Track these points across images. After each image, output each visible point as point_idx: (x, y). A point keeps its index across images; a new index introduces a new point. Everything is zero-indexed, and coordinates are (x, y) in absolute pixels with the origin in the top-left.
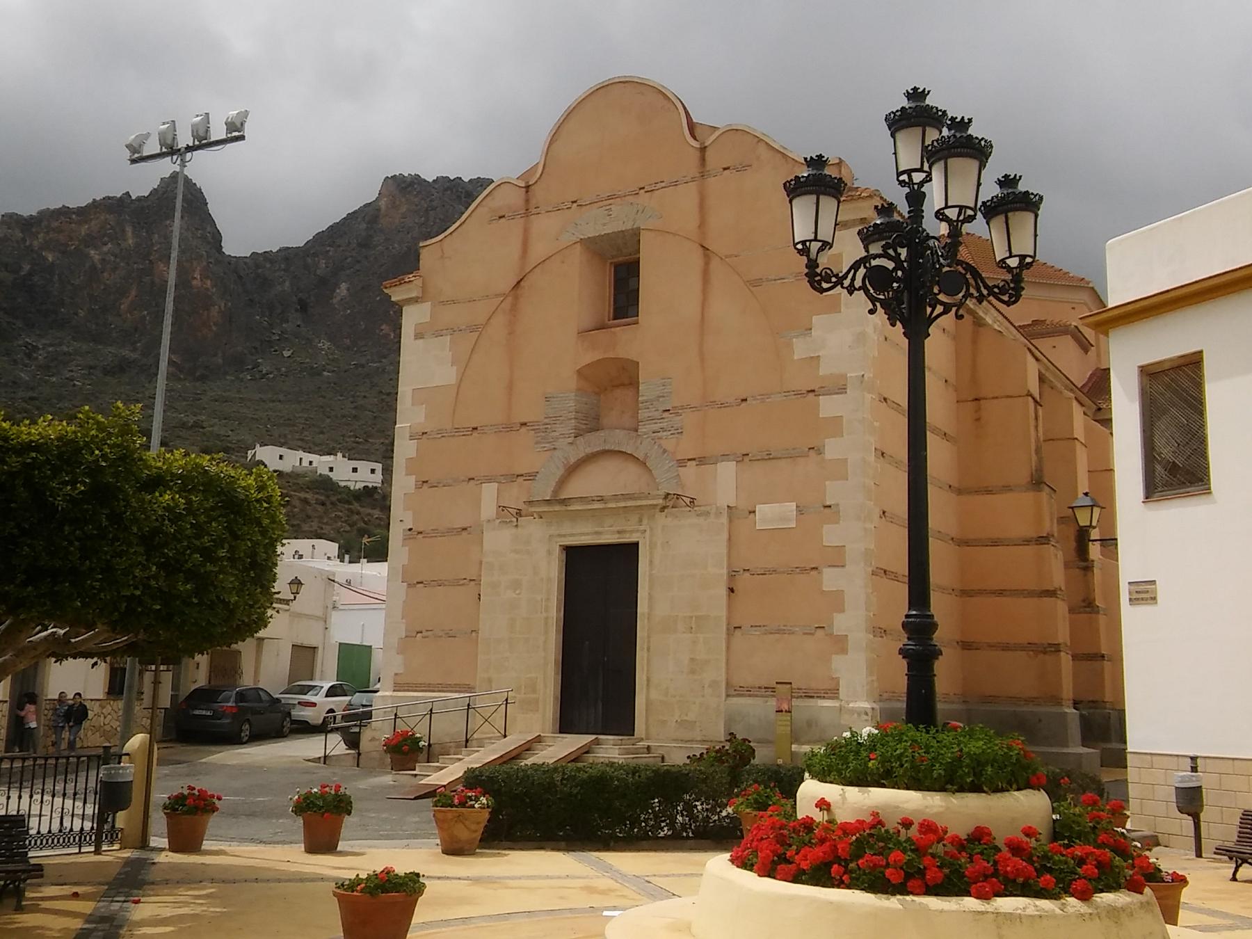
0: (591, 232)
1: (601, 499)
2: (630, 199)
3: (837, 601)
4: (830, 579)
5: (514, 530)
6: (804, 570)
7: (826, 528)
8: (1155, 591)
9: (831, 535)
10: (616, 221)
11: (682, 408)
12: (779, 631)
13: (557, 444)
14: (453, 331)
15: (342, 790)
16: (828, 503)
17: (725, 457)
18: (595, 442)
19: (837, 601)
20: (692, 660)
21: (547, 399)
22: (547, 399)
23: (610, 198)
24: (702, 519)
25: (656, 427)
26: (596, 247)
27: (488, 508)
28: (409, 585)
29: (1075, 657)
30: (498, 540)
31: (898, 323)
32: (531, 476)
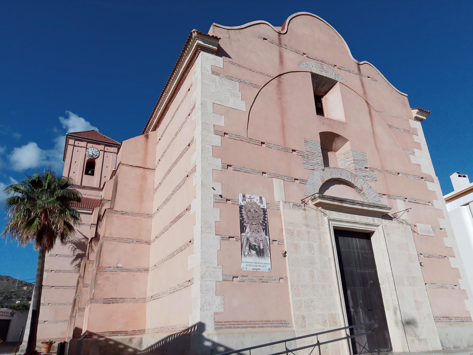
0: (315, 71)
11: (374, 169)
16: (441, 228)
17: (399, 197)
20: (416, 301)
22: (306, 142)
28: (223, 239)
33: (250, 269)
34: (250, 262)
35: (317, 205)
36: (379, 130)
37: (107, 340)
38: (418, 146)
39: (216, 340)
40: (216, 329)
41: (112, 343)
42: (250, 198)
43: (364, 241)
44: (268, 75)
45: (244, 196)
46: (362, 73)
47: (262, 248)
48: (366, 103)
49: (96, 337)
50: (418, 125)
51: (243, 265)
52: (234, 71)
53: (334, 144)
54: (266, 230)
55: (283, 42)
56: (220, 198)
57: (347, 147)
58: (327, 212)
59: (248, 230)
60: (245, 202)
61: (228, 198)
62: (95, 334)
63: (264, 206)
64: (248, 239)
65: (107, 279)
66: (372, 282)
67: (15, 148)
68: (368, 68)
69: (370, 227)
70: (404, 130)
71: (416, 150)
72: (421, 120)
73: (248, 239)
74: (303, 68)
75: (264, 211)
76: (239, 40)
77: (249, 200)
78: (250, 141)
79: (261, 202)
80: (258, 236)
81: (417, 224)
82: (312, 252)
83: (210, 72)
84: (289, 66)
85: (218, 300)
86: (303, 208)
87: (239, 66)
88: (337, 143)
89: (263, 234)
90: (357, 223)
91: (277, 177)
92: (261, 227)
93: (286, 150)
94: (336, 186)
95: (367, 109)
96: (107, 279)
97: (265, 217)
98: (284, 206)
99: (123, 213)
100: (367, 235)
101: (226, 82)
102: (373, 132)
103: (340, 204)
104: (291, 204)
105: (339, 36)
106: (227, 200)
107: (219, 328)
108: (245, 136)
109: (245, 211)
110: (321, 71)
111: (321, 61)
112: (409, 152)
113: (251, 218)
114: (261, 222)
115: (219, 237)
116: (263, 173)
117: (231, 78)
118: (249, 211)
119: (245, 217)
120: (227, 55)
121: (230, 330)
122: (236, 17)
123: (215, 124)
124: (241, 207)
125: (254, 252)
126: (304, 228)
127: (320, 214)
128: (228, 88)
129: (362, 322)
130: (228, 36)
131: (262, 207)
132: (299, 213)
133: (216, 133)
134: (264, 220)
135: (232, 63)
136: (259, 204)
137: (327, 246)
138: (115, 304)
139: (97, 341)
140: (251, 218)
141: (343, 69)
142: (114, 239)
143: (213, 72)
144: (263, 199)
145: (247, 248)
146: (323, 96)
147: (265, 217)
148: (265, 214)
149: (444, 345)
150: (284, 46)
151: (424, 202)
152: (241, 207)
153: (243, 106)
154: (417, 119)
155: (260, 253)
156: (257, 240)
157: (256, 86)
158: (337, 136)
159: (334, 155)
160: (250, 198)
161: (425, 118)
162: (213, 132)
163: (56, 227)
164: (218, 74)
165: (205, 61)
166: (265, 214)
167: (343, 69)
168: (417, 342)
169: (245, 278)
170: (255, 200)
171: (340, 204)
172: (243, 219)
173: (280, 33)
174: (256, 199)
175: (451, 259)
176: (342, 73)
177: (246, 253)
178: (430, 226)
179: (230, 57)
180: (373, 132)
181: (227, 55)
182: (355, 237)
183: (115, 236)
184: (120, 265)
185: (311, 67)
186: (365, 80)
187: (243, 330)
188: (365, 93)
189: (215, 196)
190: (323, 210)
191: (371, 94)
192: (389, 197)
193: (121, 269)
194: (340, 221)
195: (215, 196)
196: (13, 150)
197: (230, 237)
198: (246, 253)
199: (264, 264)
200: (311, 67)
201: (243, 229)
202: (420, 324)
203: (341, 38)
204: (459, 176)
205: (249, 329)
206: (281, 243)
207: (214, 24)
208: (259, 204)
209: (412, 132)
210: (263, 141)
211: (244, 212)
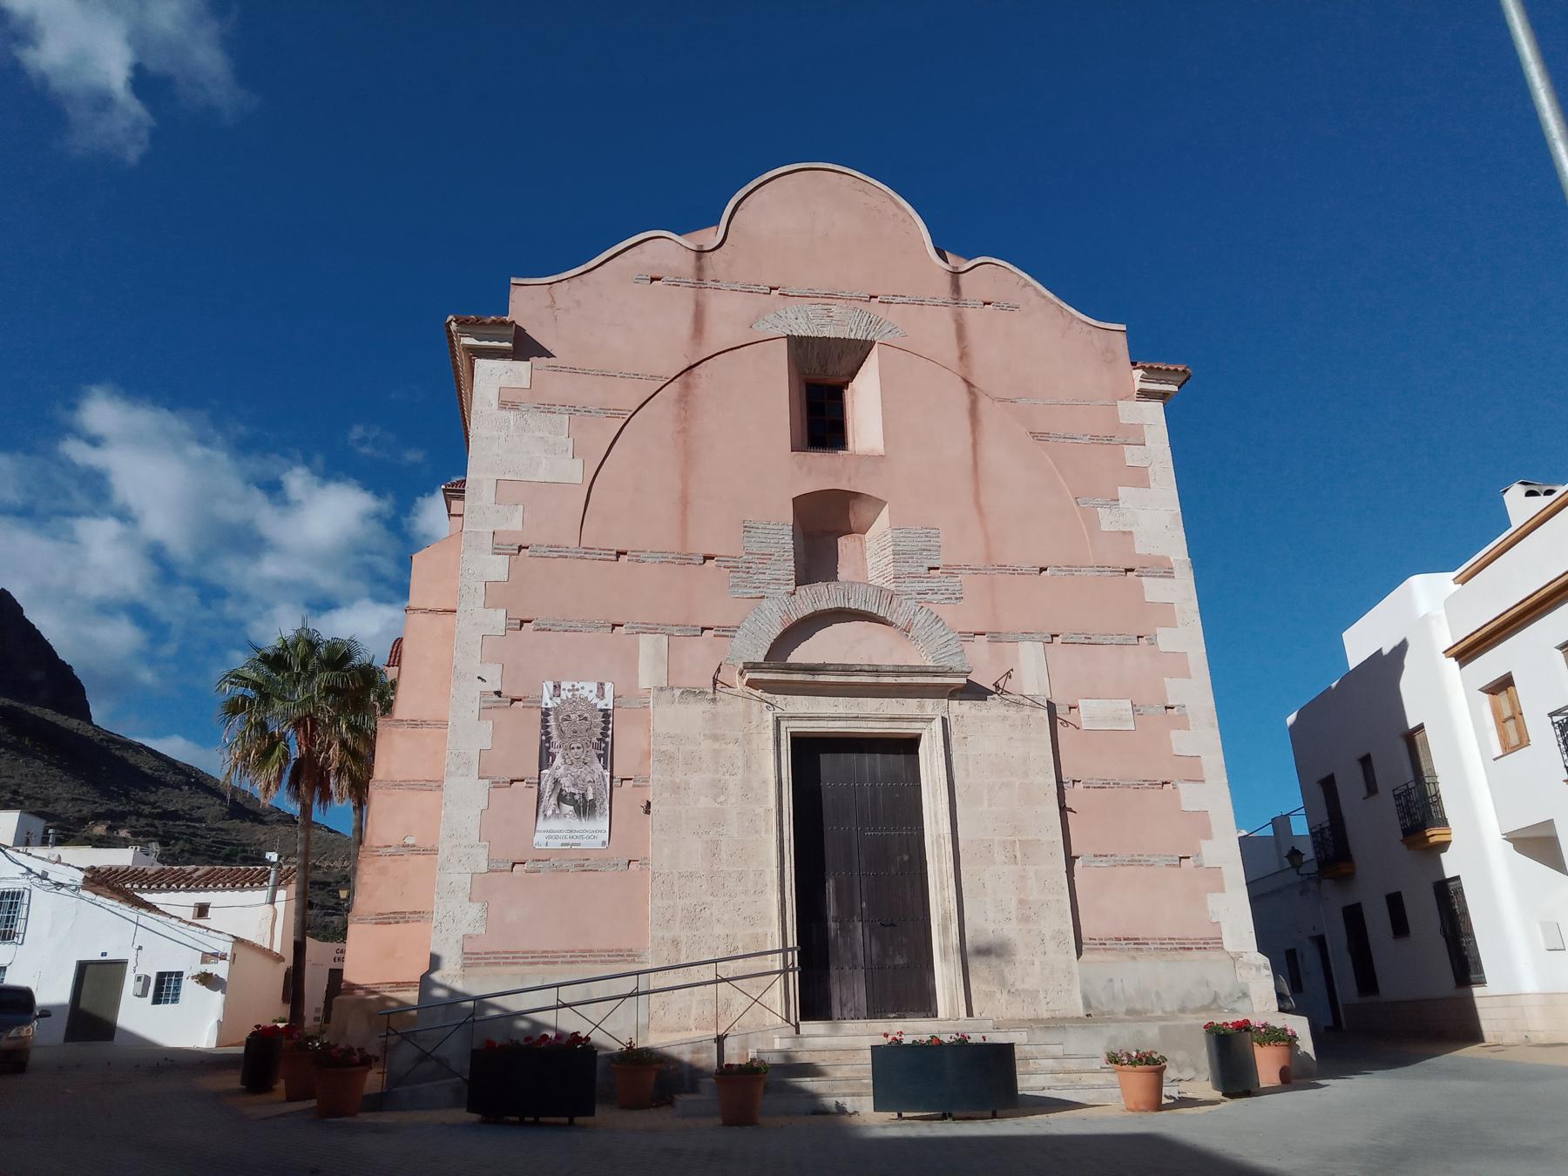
0: (802, 330)
1: (876, 671)
2: (860, 305)
3: (1201, 824)
4: (1190, 796)
5: (707, 706)
6: (1153, 784)
7: (1174, 734)
8: (166, 1001)
9: (1182, 742)
10: (839, 325)
11: (959, 567)
12: (1132, 863)
13: (768, 591)
14: (573, 410)
15: (1117, 985)
16: (1170, 704)
17: (1028, 635)
18: (819, 597)
19: (1201, 824)
20: (1021, 902)
21: (747, 529)
22: (747, 529)
23: (828, 296)
24: (1012, 712)
25: (923, 586)
26: (799, 347)
27: (648, 675)
28: (496, 785)
29: (1215, 943)
30: (677, 720)
31: (1123, 492)
32: (726, 632)
33: (555, 844)
34: (559, 831)
35: (752, 684)
36: (996, 454)
37: (384, 999)
38: (1140, 478)
39: (459, 986)
40: (464, 966)
41: (393, 1004)
42: (573, 689)
43: (896, 761)
44: (653, 377)
45: (557, 687)
46: (964, 296)
47: (590, 797)
48: (963, 385)
49: (361, 993)
50: (1154, 412)
51: (540, 839)
52: (559, 387)
53: (851, 516)
54: (606, 756)
55: (709, 274)
56: (496, 698)
57: (883, 521)
58: (779, 699)
59: (558, 761)
60: (558, 700)
61: (515, 695)
62: (360, 987)
63: (607, 702)
64: (556, 782)
65: (383, 871)
66: (906, 858)
67: (419, 499)
68: (992, 277)
69: (905, 725)
70: (1093, 437)
71: (1123, 492)
72: (1163, 396)
73: (556, 782)
74: (765, 329)
75: (606, 714)
76: (578, 302)
77: (570, 695)
78: (586, 553)
79: (601, 695)
80: (583, 772)
81: (1081, 703)
82: (722, 799)
83: (495, 404)
84: (721, 332)
85: (474, 910)
86: (710, 696)
87: (574, 370)
88: (858, 514)
89: (598, 766)
90: (864, 719)
91: (653, 630)
92: (593, 752)
93: (685, 559)
94: (837, 628)
95: (963, 399)
96: (383, 871)
97: (606, 729)
98: (656, 698)
99: (415, 724)
100: (909, 745)
101: (536, 420)
102: (975, 464)
103: (809, 678)
104: (677, 692)
105: (897, 204)
106: (513, 701)
107: (471, 965)
108: (574, 544)
109: (556, 719)
110: (823, 326)
111: (828, 296)
112: (1100, 501)
113: (569, 734)
114: (594, 740)
115: (486, 782)
116: (614, 626)
117: (547, 408)
118: (567, 719)
119: (554, 733)
120: (544, 353)
121: (496, 969)
122: (569, 245)
123: (497, 529)
124: (546, 713)
125: (568, 808)
126: (707, 745)
127: (756, 706)
128: (538, 434)
129: (860, 953)
130: (548, 301)
131: (601, 705)
132: (696, 711)
133: (497, 551)
134: (604, 735)
135: (555, 368)
136: (595, 701)
137: (765, 782)
138: (401, 925)
139: (363, 1002)
140: (569, 734)
141: (898, 299)
142: (397, 785)
143: (503, 405)
144: (608, 687)
145: (553, 800)
146: (846, 385)
147: (606, 729)
148: (606, 722)
149: (1094, 1003)
150: (710, 284)
151: (1117, 639)
152: (546, 713)
153: (575, 472)
154: (1145, 395)
155: (585, 808)
156: (580, 782)
157: (613, 414)
158: (856, 495)
159: (858, 543)
160: (573, 689)
161: (1174, 388)
162: (490, 547)
163: (327, 759)
164: (514, 406)
165: (491, 379)
166: (606, 722)
167: (898, 299)
168: (1002, 998)
169: (541, 865)
170: (585, 693)
171: (809, 678)
172: (548, 740)
173: (700, 252)
174: (588, 689)
175: (1182, 787)
176: (891, 315)
177: (549, 813)
178: (1127, 704)
179: (550, 355)
180: (975, 464)
181: (544, 353)
182: (862, 751)
183: (398, 777)
184: (410, 841)
185: (793, 322)
186: (973, 316)
187: (527, 968)
188: (963, 355)
189: (483, 694)
190: (766, 696)
191: (987, 355)
192: (995, 637)
193: (413, 849)
194: (810, 719)
195: (483, 694)
196: (414, 501)
197: (512, 782)
198: (549, 813)
199: (593, 833)
200: (793, 322)
201: (545, 759)
202: (1021, 955)
203: (904, 209)
204: (1530, 494)
205: (541, 966)
206: (641, 783)
207: (513, 280)
208: (595, 701)
209: (1135, 436)
210: (621, 549)
211: (552, 723)
